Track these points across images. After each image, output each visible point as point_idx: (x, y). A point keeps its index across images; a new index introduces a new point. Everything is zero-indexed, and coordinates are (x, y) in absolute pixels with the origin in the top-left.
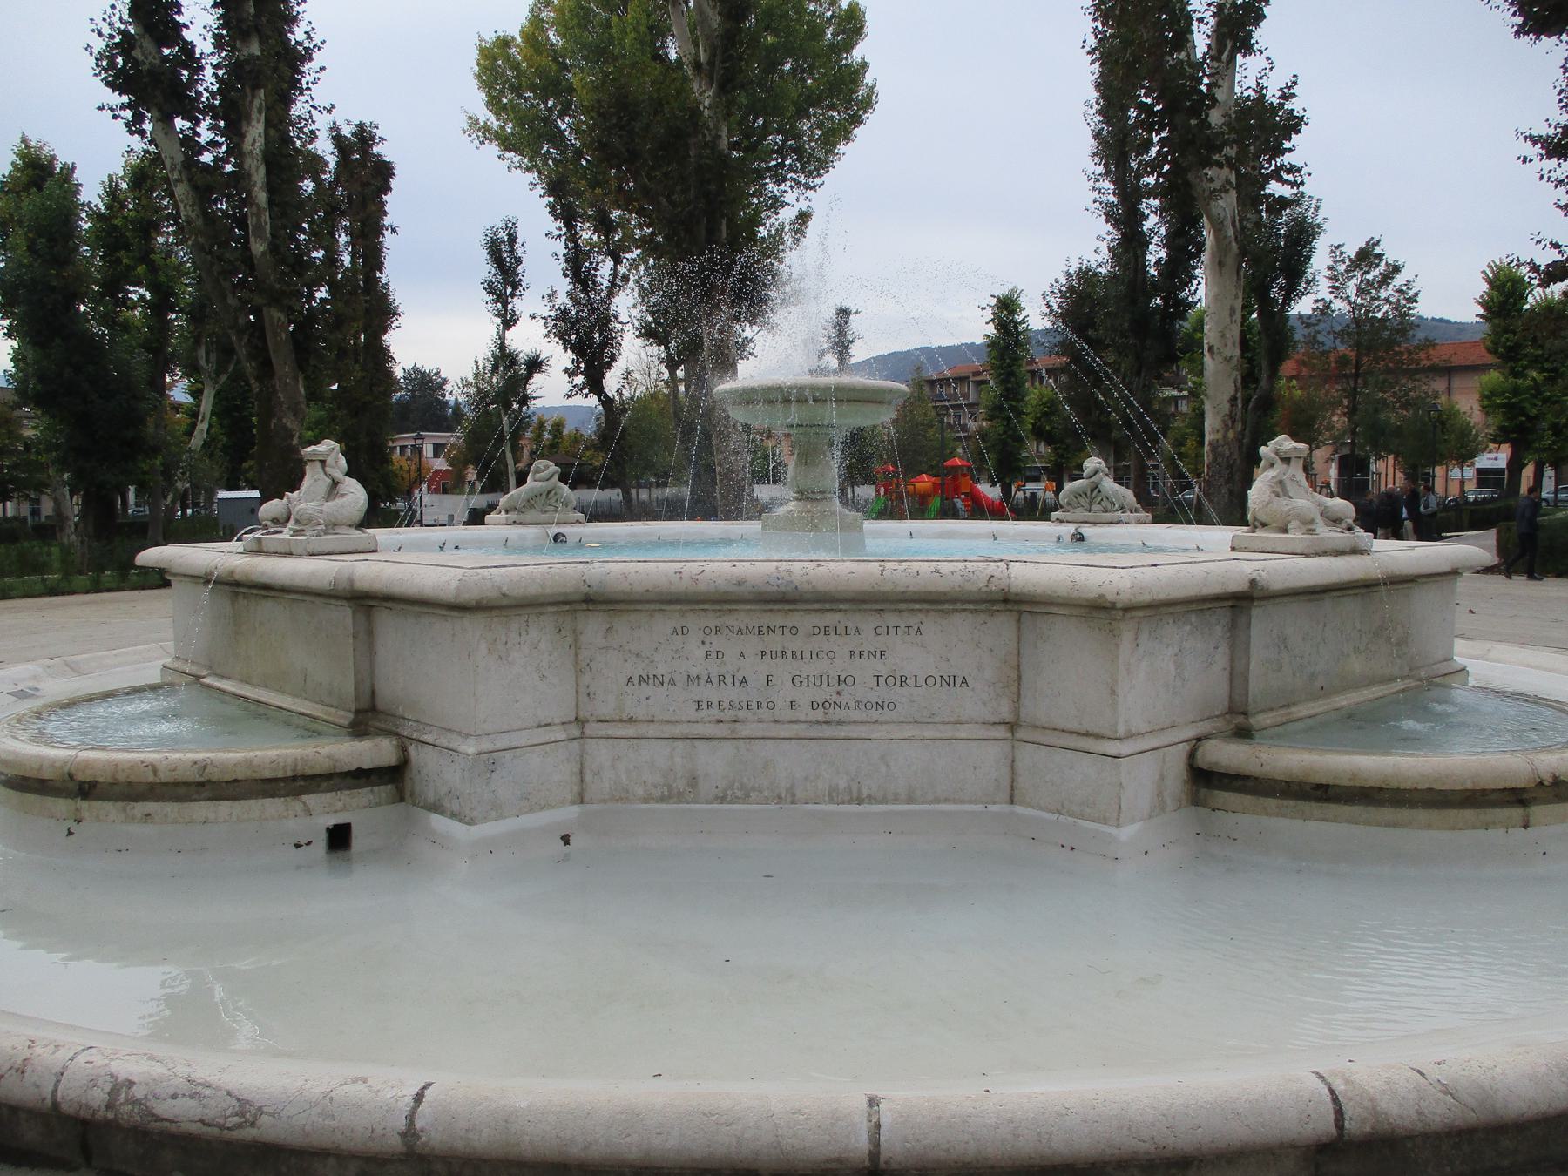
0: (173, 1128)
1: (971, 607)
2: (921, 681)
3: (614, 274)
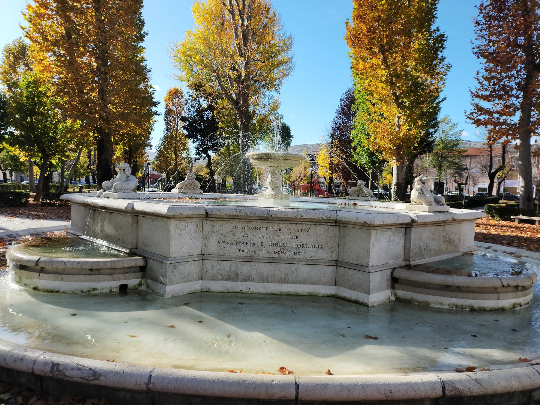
0: (71, 380)
2: (308, 246)
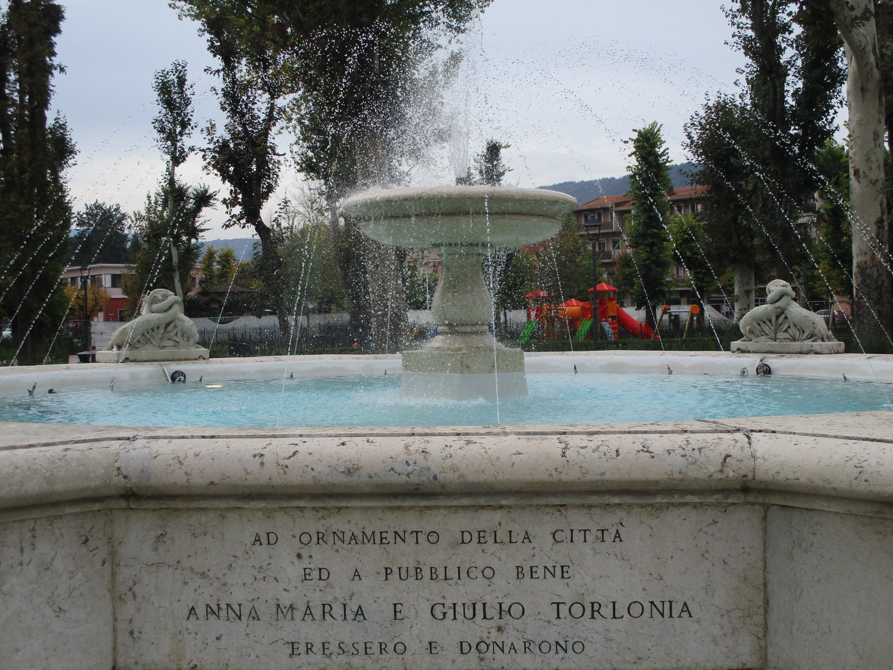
1: (696, 499)
2: (621, 610)
3: (272, 108)
